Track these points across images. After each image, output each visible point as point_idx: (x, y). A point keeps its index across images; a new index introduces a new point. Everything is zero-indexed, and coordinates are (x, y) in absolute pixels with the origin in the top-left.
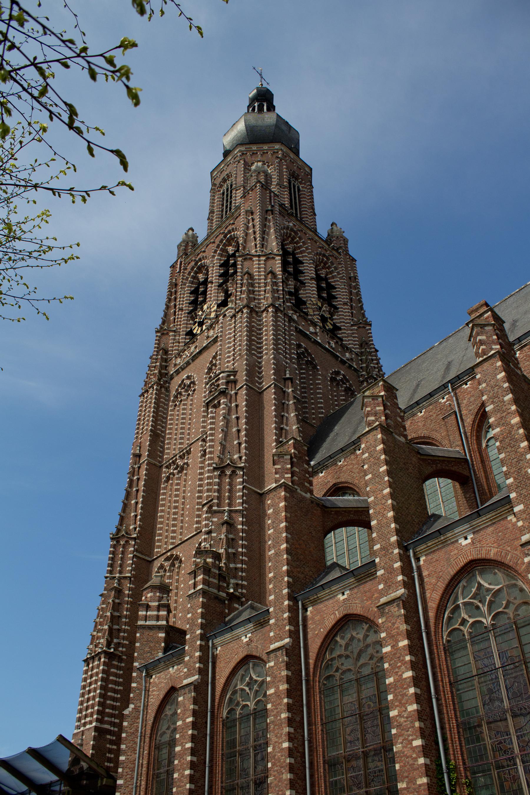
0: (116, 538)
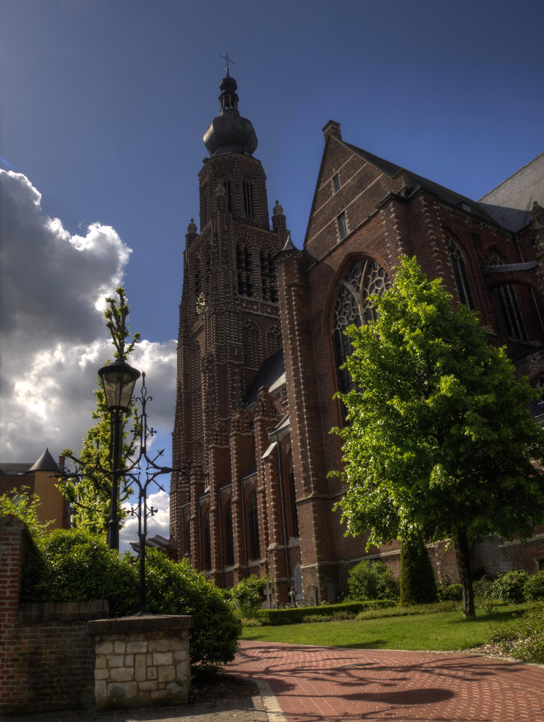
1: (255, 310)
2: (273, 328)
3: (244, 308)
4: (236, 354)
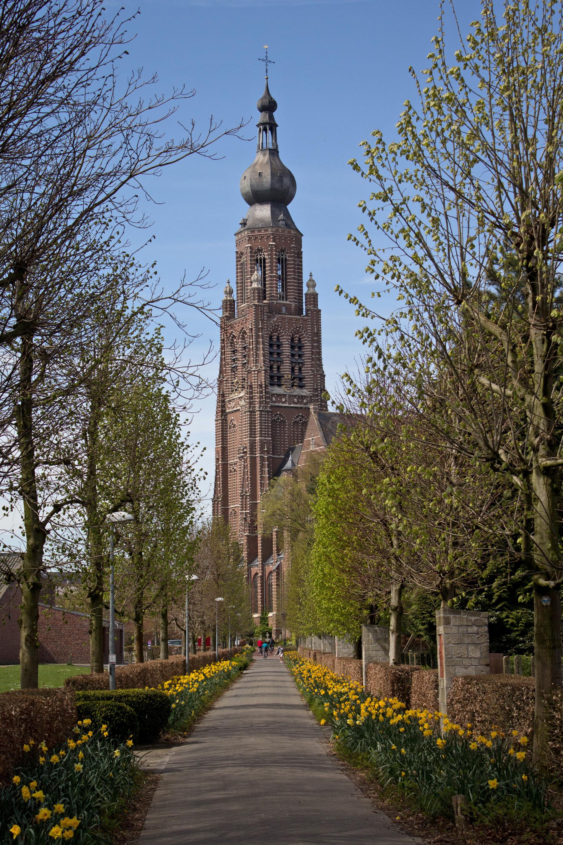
0: (214, 501)
1: (283, 403)
2: (299, 416)
3: (275, 402)
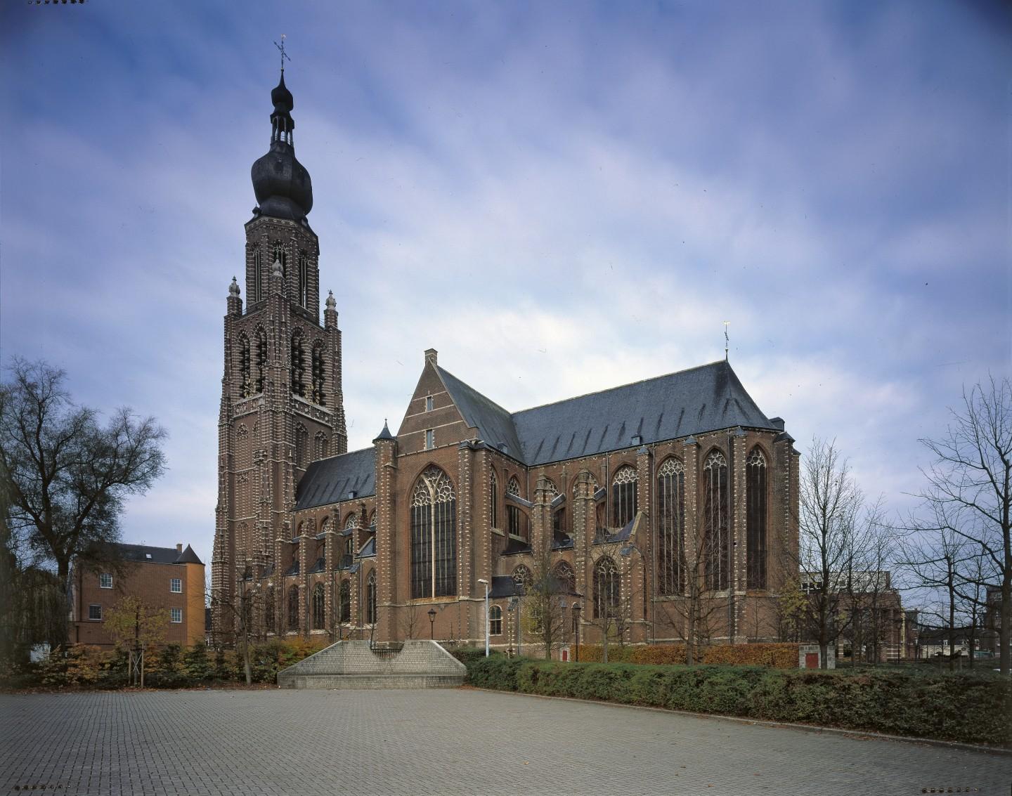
1: (306, 413)
4: (290, 455)
